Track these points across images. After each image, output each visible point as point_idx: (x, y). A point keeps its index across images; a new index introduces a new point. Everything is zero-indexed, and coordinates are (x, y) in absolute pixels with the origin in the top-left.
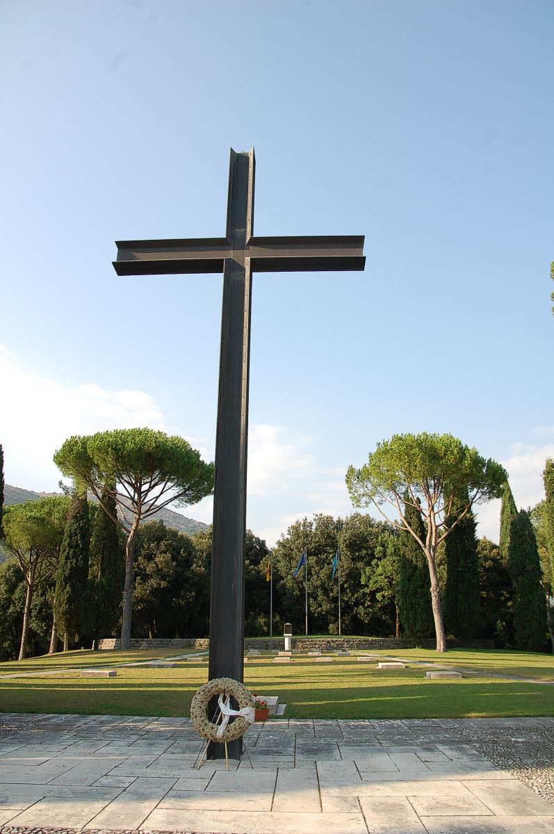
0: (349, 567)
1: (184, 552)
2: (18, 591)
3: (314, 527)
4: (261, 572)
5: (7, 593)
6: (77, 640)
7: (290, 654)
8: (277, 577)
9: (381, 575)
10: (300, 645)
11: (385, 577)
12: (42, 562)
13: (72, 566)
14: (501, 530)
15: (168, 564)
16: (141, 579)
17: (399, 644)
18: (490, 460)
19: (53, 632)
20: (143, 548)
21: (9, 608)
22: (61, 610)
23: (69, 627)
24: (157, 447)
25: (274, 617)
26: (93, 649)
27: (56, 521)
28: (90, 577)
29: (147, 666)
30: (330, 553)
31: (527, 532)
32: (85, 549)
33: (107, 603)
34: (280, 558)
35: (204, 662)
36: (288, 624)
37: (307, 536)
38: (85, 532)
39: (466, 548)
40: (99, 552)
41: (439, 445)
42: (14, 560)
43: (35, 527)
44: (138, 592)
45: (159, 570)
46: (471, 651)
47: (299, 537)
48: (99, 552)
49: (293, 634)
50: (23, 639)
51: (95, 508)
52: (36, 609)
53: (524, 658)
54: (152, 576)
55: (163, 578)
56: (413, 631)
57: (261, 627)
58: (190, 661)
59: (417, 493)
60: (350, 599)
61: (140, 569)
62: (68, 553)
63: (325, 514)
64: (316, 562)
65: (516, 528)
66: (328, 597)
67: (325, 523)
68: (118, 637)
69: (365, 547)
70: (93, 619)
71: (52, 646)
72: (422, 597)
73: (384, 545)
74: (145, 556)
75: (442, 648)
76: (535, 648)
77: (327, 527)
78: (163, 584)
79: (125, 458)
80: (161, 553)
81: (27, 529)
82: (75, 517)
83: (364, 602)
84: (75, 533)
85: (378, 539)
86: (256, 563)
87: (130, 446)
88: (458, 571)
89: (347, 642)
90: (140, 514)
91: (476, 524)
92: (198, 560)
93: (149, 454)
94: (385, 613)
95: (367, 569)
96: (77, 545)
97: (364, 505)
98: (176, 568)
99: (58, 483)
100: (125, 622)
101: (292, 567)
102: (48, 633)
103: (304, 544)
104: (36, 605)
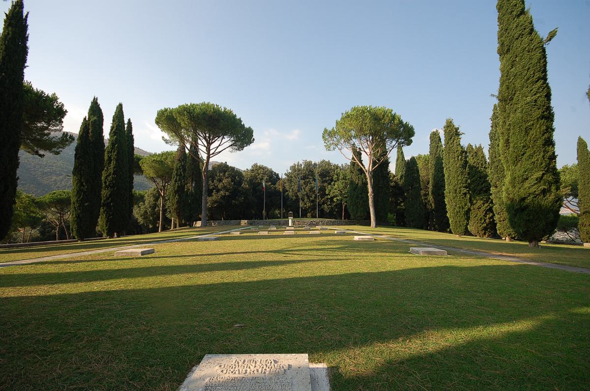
3: (303, 166)
8: (285, 191)
9: (336, 189)
13: (178, 185)
18: (407, 123)
20: (217, 176)
22: (174, 207)
24: (214, 112)
25: (283, 210)
28: (186, 190)
37: (299, 170)
41: (379, 112)
45: (225, 187)
49: (294, 218)
54: (221, 190)
55: (227, 190)
57: (277, 215)
62: (176, 179)
63: (308, 160)
64: (304, 182)
66: (310, 200)
67: (308, 164)
75: (374, 225)
77: (309, 166)
78: (227, 193)
87: (198, 111)
93: (211, 117)
96: (181, 174)
99: (162, 138)
103: (298, 174)
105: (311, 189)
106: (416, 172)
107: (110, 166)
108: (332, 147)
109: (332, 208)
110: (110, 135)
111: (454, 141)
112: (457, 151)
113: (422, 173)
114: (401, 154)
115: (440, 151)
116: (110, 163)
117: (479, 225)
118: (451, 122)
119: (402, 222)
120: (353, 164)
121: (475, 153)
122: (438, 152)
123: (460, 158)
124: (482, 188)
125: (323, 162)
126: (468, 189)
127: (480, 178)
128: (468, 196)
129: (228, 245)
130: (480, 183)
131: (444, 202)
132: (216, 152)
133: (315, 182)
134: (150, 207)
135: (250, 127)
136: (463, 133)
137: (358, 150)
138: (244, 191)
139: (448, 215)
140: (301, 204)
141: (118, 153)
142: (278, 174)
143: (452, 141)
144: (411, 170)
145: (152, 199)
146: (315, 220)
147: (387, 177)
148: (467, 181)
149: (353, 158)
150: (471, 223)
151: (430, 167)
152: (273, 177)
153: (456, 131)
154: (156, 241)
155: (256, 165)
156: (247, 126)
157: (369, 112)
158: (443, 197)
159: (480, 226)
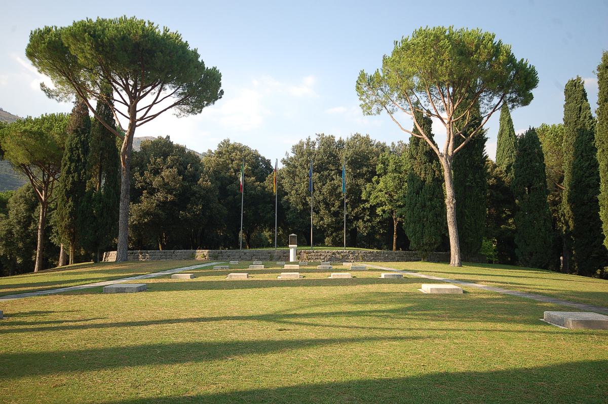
0: (350, 183)
1: (191, 167)
3: (316, 146)
4: (267, 187)
6: (83, 252)
7: (297, 267)
8: (282, 193)
9: (381, 191)
11: (386, 193)
13: (73, 180)
14: (498, 152)
15: (174, 178)
16: (147, 193)
20: (149, 162)
21: (29, 225)
22: (63, 224)
25: (278, 231)
28: (87, 189)
30: (332, 170)
31: (536, 150)
34: (284, 175)
36: (293, 235)
37: (310, 154)
41: (468, 40)
45: (166, 184)
47: (302, 155)
49: (299, 245)
54: (158, 190)
55: (170, 192)
56: (419, 244)
57: (267, 239)
60: (351, 213)
61: (146, 183)
62: (69, 168)
63: (327, 134)
65: (524, 145)
66: (330, 211)
67: (328, 142)
69: (365, 165)
71: (36, 266)
72: (430, 211)
73: (385, 162)
74: (151, 171)
75: (457, 262)
76: (538, 265)
79: (107, 47)
80: (167, 168)
82: (76, 131)
83: (364, 217)
84: (76, 147)
85: (378, 157)
86: (261, 179)
87: (111, 33)
89: (352, 253)
91: (486, 140)
93: (137, 45)
94: (382, 227)
95: (368, 185)
96: (79, 160)
97: (375, 112)
103: (308, 162)
105: (334, 191)
106: (538, 158)
108: (375, 107)
113: (550, 161)
114: (507, 124)
115: (585, 117)
120: (416, 141)
122: (581, 119)
125: (357, 137)
131: (598, 216)
134: (19, 223)
137: (425, 115)
138: (203, 193)
140: (314, 220)
144: (529, 154)
145: (23, 207)
146: (339, 249)
147: (481, 168)
149: (415, 130)
155: (226, 143)
156: (209, 65)
157: (449, 38)
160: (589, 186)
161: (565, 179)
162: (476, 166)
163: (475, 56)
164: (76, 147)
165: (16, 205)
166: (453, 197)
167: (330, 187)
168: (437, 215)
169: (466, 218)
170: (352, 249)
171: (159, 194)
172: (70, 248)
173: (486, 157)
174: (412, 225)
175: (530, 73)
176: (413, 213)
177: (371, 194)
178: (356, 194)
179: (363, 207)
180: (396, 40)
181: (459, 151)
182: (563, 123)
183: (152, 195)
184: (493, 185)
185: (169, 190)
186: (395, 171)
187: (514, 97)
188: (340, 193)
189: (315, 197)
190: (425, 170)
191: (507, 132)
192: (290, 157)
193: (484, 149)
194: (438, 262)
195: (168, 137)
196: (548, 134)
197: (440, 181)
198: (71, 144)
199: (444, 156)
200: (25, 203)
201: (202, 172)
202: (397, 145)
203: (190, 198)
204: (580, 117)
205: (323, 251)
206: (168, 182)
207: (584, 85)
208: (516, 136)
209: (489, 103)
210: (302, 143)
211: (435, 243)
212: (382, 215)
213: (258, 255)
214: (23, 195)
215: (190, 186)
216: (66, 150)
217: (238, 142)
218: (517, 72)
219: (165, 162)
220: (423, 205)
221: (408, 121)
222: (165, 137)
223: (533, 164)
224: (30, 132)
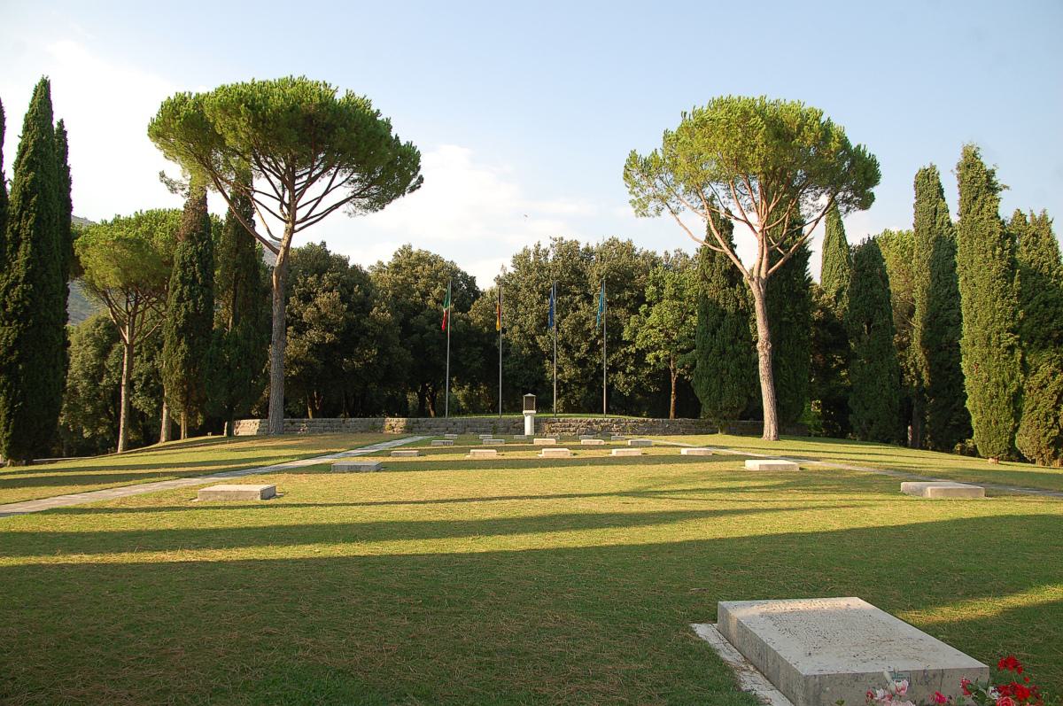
1: (359, 290)
2: (113, 355)
3: (550, 257)
5: (97, 358)
6: (200, 421)
9: (652, 327)
10: (547, 427)
12: (143, 311)
17: (690, 427)
18: (859, 147)
19: (165, 411)
20: (297, 284)
21: (101, 380)
22: (174, 378)
23: (187, 402)
24: (322, 105)
26: (225, 434)
27: (161, 245)
28: (216, 326)
29: (328, 469)
30: (575, 294)
31: (878, 270)
32: (206, 286)
33: (243, 366)
35: (419, 459)
36: (530, 395)
37: (541, 268)
38: (205, 261)
39: (794, 288)
40: (228, 286)
41: (787, 117)
42: (105, 312)
43: (127, 254)
44: (292, 349)
45: (323, 317)
46: (814, 441)
48: (228, 286)
50: (122, 423)
51: (218, 226)
52: (140, 380)
53: (879, 451)
56: (716, 408)
58: (398, 455)
59: (727, 202)
61: (292, 315)
62: (181, 293)
63: (568, 238)
65: (862, 262)
66: (572, 358)
68: (263, 414)
70: (223, 390)
72: (732, 359)
74: (300, 295)
75: (772, 434)
76: (880, 437)
78: (329, 337)
80: (324, 292)
81: (116, 256)
82: (191, 237)
84: (191, 262)
85: (647, 274)
86: (465, 309)
87: (276, 102)
88: (782, 322)
89: (616, 423)
90: (294, 223)
92: (381, 302)
93: (309, 118)
94: (653, 384)
95: (633, 318)
96: (195, 281)
97: (653, 213)
98: (346, 314)
100: (274, 394)
101: (518, 313)
102: (159, 412)
104: (141, 375)
106: (881, 282)
107: (16, 258)
108: (653, 204)
109: (639, 384)
110: (15, 170)
111: (982, 207)
112: (991, 233)
113: (896, 285)
114: (837, 232)
115: (942, 224)
116: (16, 248)
117: (1042, 431)
118: (974, 155)
119: (837, 427)
120: (710, 255)
121: (1034, 235)
122: (938, 226)
123: (997, 252)
124: (1050, 333)
125: (613, 243)
126: (1018, 336)
127: (1046, 304)
128: (1018, 354)
129: (529, 480)
130: (1046, 318)
131: (960, 368)
132: (313, 214)
133: (590, 303)
134: (86, 375)
135: (630, 242)
136: (1005, 187)
137: (723, 216)
138: (379, 330)
139: (969, 405)
141: (38, 221)
142: (473, 279)
143: (978, 207)
144: (869, 276)
145: (91, 352)
146: (598, 417)
147: (804, 295)
148: (1015, 313)
149: (710, 238)
150: (1024, 424)
151: (915, 269)
152: (464, 289)
153: (989, 180)
154: (165, 474)
155: (406, 251)
158: (954, 350)
159: (1045, 435)
160: (947, 323)
161: (917, 312)
162: (796, 293)
163: (797, 140)
164: (191, 262)
165: (81, 348)
166: (767, 339)
167: (573, 321)
168: (741, 366)
169: (782, 369)
170: (617, 417)
171: (312, 332)
172: (182, 414)
173: (810, 279)
174: (705, 380)
175: (870, 165)
176: (708, 363)
177: (637, 332)
178: (614, 331)
179: (625, 351)
180: (684, 111)
181: (775, 272)
182: (913, 230)
183: (301, 333)
184: (818, 320)
185: (327, 326)
186: (674, 297)
187: (849, 196)
188: (589, 330)
189: (549, 337)
190: (725, 298)
191: (836, 240)
192: (507, 273)
193: (808, 267)
194: (741, 434)
195: (324, 244)
196: (893, 245)
197: (745, 315)
198: (183, 257)
199: (756, 280)
200: (94, 346)
201: (376, 298)
202: (672, 255)
203: (359, 338)
204: (935, 223)
205: (574, 419)
206: (326, 314)
207: (940, 177)
208: (848, 247)
209: (814, 204)
210: (526, 252)
211: (738, 408)
212: (654, 365)
213: (475, 426)
214: (91, 332)
215: (358, 319)
216: (176, 265)
217: (424, 248)
218: (853, 163)
219: (321, 282)
220: (722, 350)
221: (698, 224)
222: (318, 244)
223: (875, 290)
224: (126, 240)
